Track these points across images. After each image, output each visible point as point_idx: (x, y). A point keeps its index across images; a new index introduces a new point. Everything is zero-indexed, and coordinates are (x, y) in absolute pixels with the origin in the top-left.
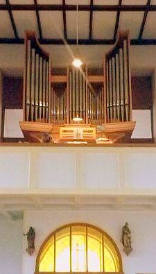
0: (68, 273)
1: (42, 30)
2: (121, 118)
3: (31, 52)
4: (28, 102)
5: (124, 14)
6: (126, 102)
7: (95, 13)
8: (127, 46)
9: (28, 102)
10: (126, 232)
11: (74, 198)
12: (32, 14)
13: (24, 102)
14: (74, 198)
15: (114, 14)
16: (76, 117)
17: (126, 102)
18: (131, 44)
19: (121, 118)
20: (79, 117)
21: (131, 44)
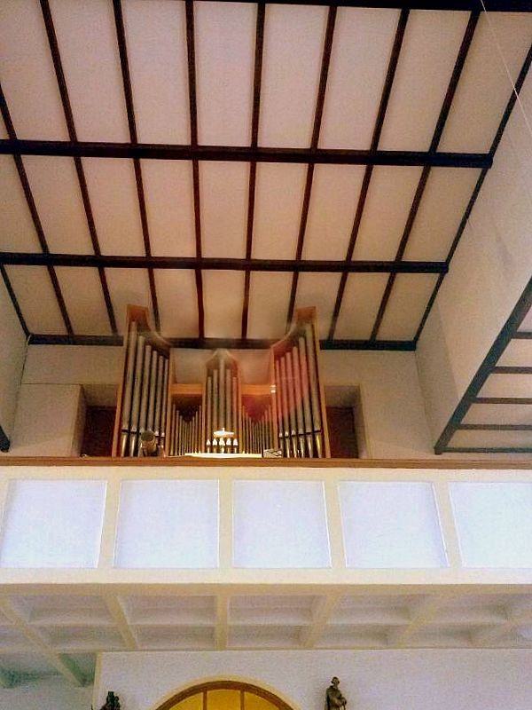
0: (492, 7)
1: (159, 302)
2: (316, 455)
3: (158, 361)
4: (125, 427)
5: (306, 278)
6: (317, 428)
7: (255, 275)
8: (315, 351)
9: (125, 427)
10: (336, 701)
11: (212, 599)
12: (140, 274)
13: (203, 442)
14: (212, 599)
15: (287, 276)
16: (218, 429)
17: (317, 428)
18: (321, 348)
19: (316, 455)
20: (226, 430)
21: (321, 348)
